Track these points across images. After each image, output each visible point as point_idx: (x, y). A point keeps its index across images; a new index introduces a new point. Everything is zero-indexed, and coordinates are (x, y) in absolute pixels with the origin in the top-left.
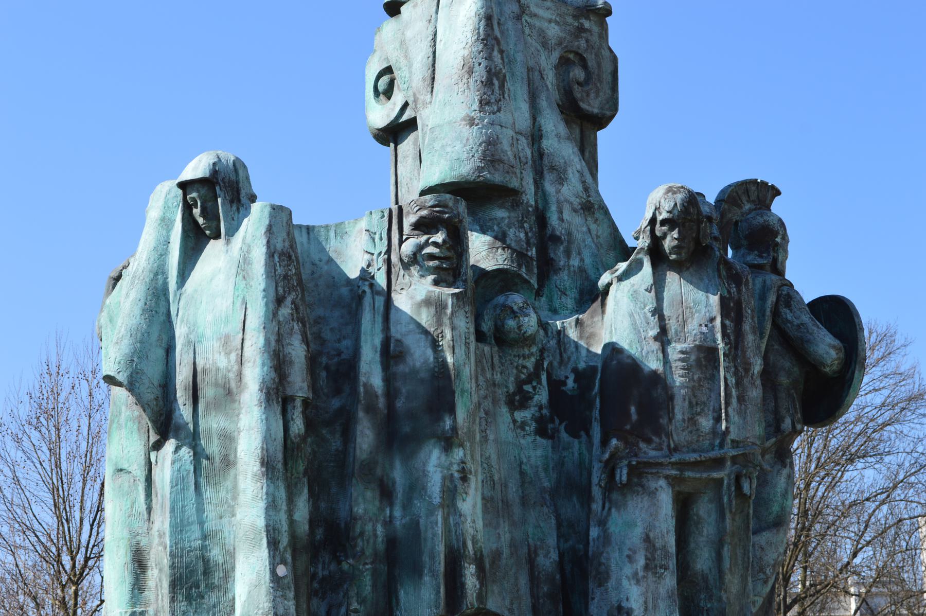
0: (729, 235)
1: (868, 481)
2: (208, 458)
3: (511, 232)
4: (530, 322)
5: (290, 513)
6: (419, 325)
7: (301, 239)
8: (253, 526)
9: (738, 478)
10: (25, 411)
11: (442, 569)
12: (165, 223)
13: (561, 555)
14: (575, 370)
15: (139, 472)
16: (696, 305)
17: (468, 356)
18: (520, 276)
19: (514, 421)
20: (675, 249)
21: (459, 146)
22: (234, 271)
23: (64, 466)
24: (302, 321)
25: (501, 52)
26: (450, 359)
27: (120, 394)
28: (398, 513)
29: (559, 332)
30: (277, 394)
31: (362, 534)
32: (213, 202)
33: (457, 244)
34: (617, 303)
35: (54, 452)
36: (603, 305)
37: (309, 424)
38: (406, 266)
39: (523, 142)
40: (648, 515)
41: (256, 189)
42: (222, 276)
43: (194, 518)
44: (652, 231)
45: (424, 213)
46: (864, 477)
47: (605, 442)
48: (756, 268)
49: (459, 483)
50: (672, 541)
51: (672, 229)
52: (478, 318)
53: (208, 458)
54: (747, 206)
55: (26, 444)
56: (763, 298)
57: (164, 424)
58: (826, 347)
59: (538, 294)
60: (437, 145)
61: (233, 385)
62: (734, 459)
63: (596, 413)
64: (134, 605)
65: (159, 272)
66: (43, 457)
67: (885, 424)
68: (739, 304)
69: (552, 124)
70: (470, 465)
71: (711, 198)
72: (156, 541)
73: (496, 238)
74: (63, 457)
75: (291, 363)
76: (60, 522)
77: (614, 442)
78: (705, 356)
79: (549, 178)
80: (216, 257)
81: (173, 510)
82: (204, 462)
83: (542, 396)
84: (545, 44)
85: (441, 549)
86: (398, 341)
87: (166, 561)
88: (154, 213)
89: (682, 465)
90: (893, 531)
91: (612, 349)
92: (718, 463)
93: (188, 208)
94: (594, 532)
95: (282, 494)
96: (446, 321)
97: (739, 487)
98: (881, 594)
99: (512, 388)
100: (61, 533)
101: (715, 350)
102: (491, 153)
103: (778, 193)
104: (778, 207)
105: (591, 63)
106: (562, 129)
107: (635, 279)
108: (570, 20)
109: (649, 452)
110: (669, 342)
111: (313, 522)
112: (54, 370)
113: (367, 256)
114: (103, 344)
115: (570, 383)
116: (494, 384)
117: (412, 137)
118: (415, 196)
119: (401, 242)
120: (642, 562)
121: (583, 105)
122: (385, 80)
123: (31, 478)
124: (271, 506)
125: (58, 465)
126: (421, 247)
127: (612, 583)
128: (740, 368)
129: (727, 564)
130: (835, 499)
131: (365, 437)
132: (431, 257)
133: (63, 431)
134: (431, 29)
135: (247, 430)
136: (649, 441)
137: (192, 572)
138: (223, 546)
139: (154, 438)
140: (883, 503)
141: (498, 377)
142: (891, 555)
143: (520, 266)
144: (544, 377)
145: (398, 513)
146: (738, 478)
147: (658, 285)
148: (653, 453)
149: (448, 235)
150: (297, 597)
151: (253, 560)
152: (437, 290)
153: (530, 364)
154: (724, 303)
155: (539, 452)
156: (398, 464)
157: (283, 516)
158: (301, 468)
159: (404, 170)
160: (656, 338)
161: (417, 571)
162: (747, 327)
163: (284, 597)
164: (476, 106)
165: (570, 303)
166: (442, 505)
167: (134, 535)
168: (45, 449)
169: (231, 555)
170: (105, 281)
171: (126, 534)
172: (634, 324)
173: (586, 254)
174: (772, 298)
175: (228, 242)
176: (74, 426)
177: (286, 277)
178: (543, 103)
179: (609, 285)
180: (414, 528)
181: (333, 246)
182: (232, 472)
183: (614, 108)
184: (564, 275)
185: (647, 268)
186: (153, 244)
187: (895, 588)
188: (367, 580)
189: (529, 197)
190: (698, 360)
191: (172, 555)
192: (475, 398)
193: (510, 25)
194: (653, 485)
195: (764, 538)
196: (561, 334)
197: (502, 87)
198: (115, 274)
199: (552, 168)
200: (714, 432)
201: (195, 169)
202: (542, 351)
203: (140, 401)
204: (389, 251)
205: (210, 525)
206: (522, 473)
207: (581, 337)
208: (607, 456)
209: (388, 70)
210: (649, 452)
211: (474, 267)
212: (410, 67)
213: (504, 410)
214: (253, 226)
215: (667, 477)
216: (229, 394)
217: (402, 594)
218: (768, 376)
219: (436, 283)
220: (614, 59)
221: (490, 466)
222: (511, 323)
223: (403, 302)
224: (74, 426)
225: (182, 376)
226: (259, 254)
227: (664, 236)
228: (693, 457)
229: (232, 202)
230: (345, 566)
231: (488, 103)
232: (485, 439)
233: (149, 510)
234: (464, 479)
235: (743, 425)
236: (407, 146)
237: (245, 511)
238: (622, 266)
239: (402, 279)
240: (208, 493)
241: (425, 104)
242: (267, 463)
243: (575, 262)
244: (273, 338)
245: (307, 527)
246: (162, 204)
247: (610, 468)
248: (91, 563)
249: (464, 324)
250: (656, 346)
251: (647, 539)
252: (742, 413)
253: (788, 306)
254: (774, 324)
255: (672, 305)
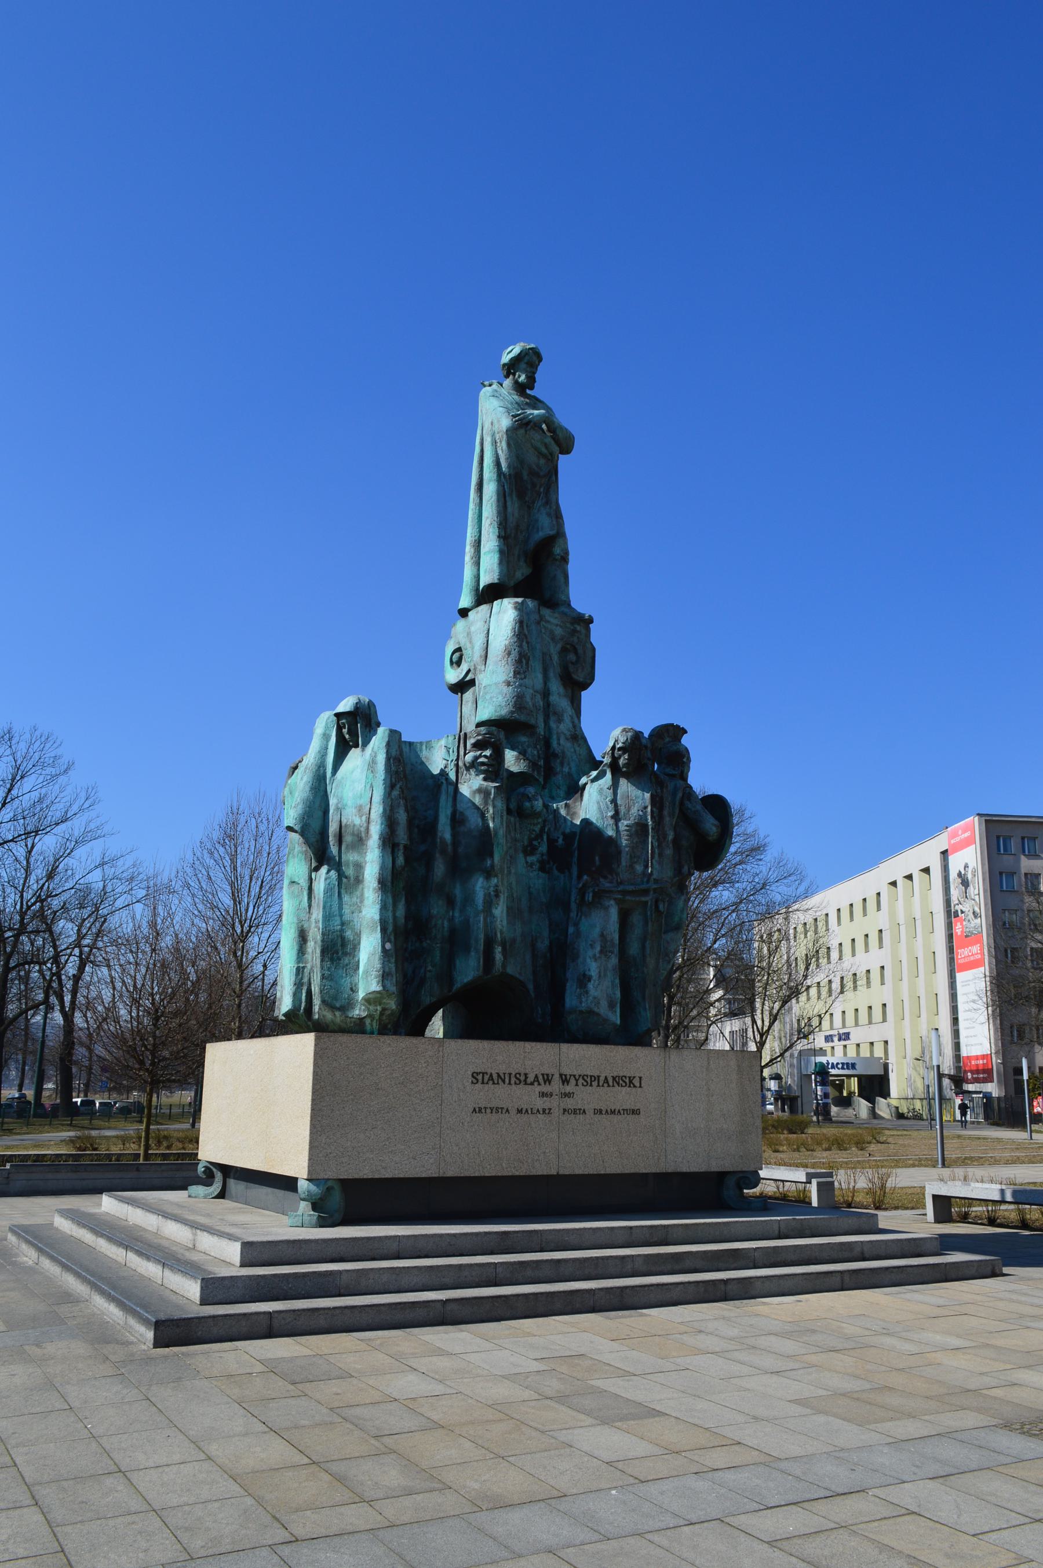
0: (655, 757)
1: (725, 898)
2: (346, 877)
3: (529, 750)
4: (539, 804)
5: (394, 912)
6: (474, 804)
7: (406, 749)
8: (372, 918)
9: (657, 902)
10: (216, 835)
11: (482, 948)
12: (326, 737)
13: (551, 943)
14: (564, 834)
15: (304, 883)
16: (637, 798)
17: (502, 823)
18: (533, 776)
19: (527, 862)
20: (625, 765)
21: (500, 698)
22: (366, 767)
23: (239, 869)
24: (405, 799)
25: (528, 643)
26: (491, 825)
27: (295, 837)
28: (457, 914)
29: (555, 811)
30: (388, 842)
31: (436, 925)
32: (354, 727)
33: (498, 757)
34: (590, 795)
35: (233, 861)
36: (582, 796)
37: (407, 859)
38: (468, 769)
39: (539, 697)
40: (603, 922)
41: (380, 719)
42: (359, 770)
43: (337, 913)
44: (613, 754)
45: (480, 737)
46: (723, 895)
47: (579, 877)
48: (672, 776)
49: (494, 898)
50: (616, 936)
51: (624, 753)
52: (508, 800)
53: (346, 877)
54: (667, 740)
55: (216, 855)
56: (674, 794)
57: (321, 853)
58: (710, 825)
59: (544, 787)
60: (488, 697)
61: (363, 835)
62: (655, 890)
63: (575, 860)
64: (298, 962)
65: (321, 765)
66: (226, 864)
67: (736, 865)
68: (662, 798)
69: (556, 686)
70: (501, 888)
71: (646, 735)
72: (313, 925)
73: (520, 753)
74: (239, 864)
75: (398, 823)
76: (235, 903)
77: (585, 877)
78: (640, 829)
79: (552, 718)
80: (355, 759)
81: (324, 908)
82: (344, 880)
83: (543, 848)
84: (553, 639)
85: (482, 936)
86: (462, 813)
87: (319, 938)
88: (319, 729)
89: (624, 893)
90: (738, 929)
91: (586, 822)
92: (646, 892)
93: (339, 729)
94: (571, 930)
95: (390, 900)
96: (490, 802)
97: (657, 907)
98: (729, 966)
99: (526, 843)
100: (235, 912)
101: (647, 825)
102: (519, 702)
103: (685, 732)
104: (685, 740)
105: (580, 651)
106: (562, 690)
107: (601, 782)
108: (568, 625)
109: (605, 884)
110: (620, 820)
111: (407, 918)
112: (235, 811)
113: (444, 762)
114: (286, 807)
115: (560, 841)
116: (516, 840)
117: (471, 690)
118: (474, 728)
119: (465, 754)
120: (598, 948)
121: (575, 677)
122: (457, 655)
123: (218, 875)
124: (383, 908)
125: (235, 869)
126: (476, 758)
127: (581, 960)
128: (660, 837)
129: (648, 951)
130: (704, 908)
131: (440, 869)
132: (483, 764)
133: (239, 849)
134: (486, 627)
135: (371, 862)
136: (605, 877)
137: (335, 944)
138: (353, 929)
139: (314, 865)
140: (733, 911)
141: (518, 836)
142: (737, 943)
143: (533, 770)
144: (545, 837)
145: (457, 914)
146: (657, 902)
147: (615, 786)
148: (608, 885)
149: (493, 751)
150: (396, 962)
151: (371, 939)
152: (485, 783)
153: (537, 828)
154: (653, 798)
155: (540, 881)
156: (458, 886)
157: (390, 914)
158: (401, 885)
159: (467, 708)
160: (612, 817)
161: (467, 949)
162: (666, 813)
163: (389, 961)
164: (511, 674)
165: (562, 793)
166: (483, 911)
167: (300, 921)
168: (227, 858)
169: (358, 935)
170: (287, 770)
171: (295, 920)
172: (599, 808)
173: (573, 765)
174: (680, 795)
175: (363, 750)
176: (247, 846)
177: (397, 772)
178: (551, 674)
179: (586, 784)
180: (467, 924)
181: (424, 754)
182: (361, 886)
183: (592, 679)
184: (559, 777)
185: (609, 775)
186: (318, 749)
187: (737, 962)
188: (438, 953)
189: (541, 730)
190: (636, 831)
191: (323, 934)
192: (505, 848)
193: (533, 627)
194: (607, 903)
195: (669, 936)
196: (556, 812)
197: (527, 663)
198: (294, 765)
199: (555, 713)
200: (644, 873)
201: (345, 705)
202: (545, 821)
203: (307, 842)
204: (457, 760)
205: (347, 917)
206: (530, 893)
207: (568, 814)
208: (581, 885)
209: (459, 650)
210: (605, 884)
211: (507, 770)
212: (473, 648)
213: (521, 855)
214: (378, 741)
215: (615, 899)
216: (360, 841)
217: (458, 962)
218: (676, 842)
219: (485, 779)
220: (594, 650)
221: (511, 888)
222: (527, 804)
223: (465, 790)
224: (247, 846)
225: (333, 828)
226: (381, 758)
227: (620, 757)
228: (631, 888)
229: (366, 726)
230: (425, 944)
231: (519, 673)
232: (509, 872)
233: (310, 906)
234: (497, 896)
235: (657, 869)
236: (468, 695)
237: (368, 908)
238: (594, 773)
239: (465, 776)
240: (346, 898)
241: (480, 671)
242: (382, 882)
243: (566, 769)
244: (388, 809)
245: (403, 921)
246: (324, 724)
247: (582, 892)
248: (252, 929)
249: (500, 804)
250: (612, 822)
251: (602, 935)
252: (660, 863)
253: (689, 800)
254: (681, 810)
255: (622, 798)
